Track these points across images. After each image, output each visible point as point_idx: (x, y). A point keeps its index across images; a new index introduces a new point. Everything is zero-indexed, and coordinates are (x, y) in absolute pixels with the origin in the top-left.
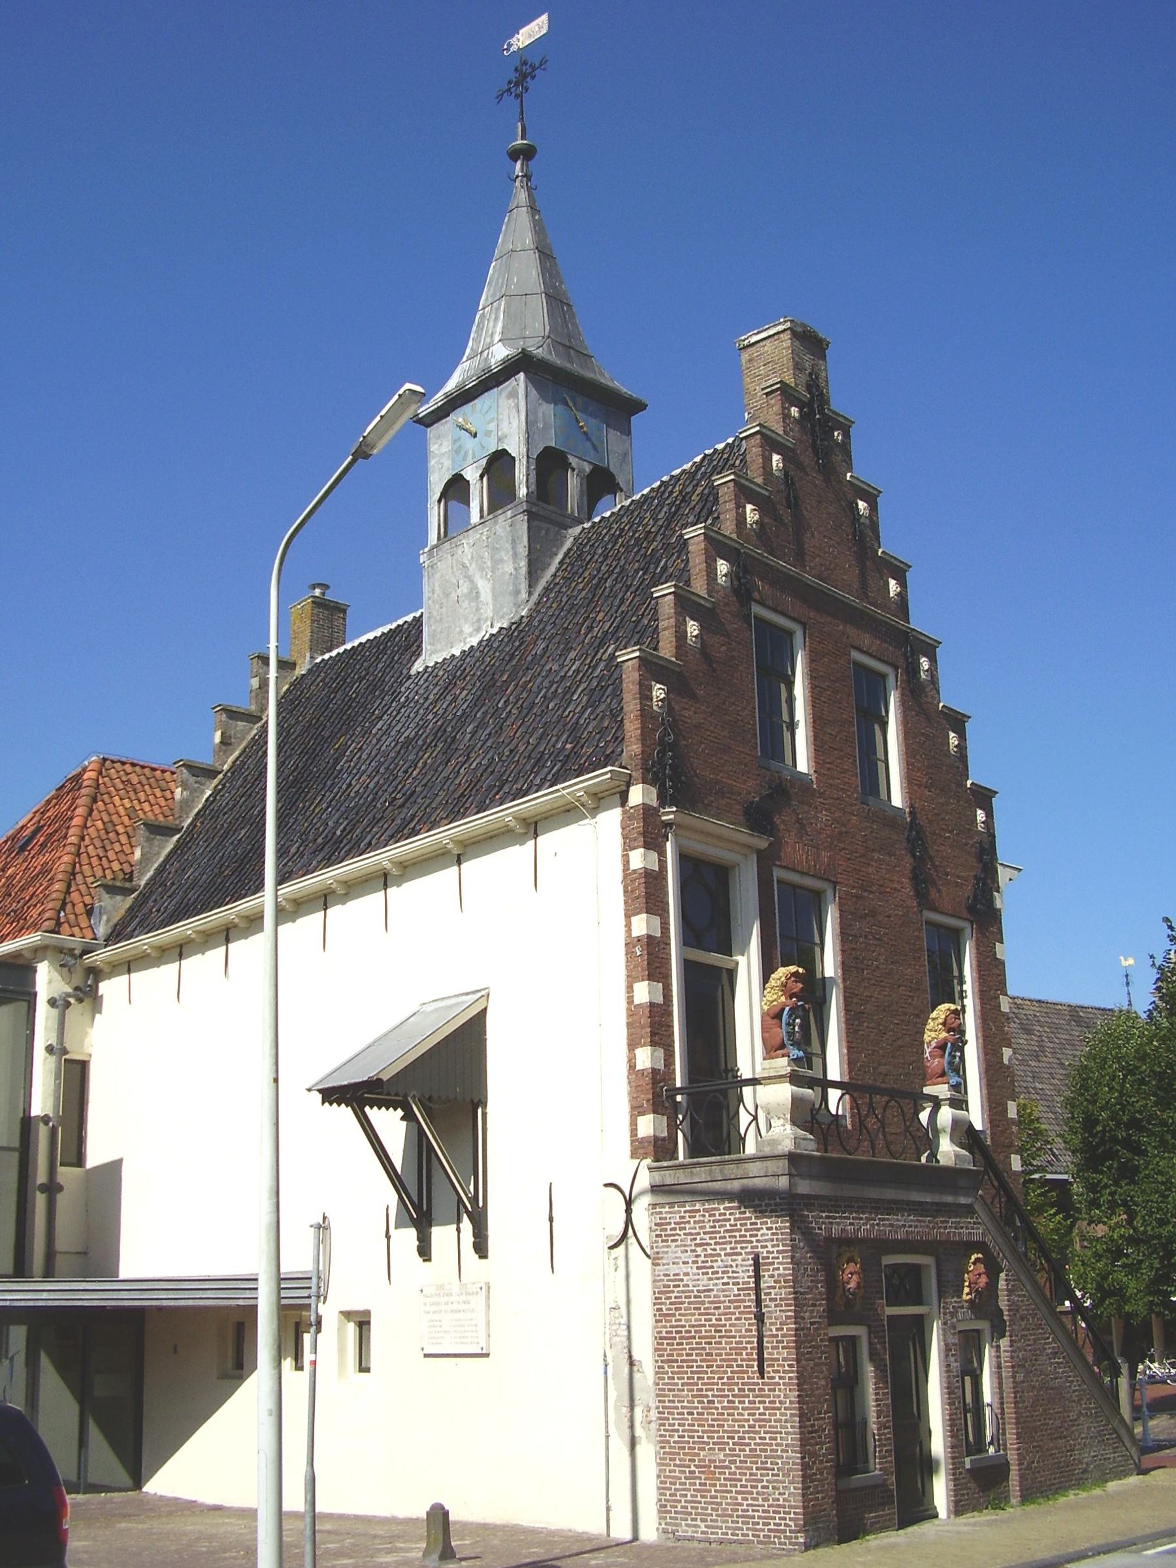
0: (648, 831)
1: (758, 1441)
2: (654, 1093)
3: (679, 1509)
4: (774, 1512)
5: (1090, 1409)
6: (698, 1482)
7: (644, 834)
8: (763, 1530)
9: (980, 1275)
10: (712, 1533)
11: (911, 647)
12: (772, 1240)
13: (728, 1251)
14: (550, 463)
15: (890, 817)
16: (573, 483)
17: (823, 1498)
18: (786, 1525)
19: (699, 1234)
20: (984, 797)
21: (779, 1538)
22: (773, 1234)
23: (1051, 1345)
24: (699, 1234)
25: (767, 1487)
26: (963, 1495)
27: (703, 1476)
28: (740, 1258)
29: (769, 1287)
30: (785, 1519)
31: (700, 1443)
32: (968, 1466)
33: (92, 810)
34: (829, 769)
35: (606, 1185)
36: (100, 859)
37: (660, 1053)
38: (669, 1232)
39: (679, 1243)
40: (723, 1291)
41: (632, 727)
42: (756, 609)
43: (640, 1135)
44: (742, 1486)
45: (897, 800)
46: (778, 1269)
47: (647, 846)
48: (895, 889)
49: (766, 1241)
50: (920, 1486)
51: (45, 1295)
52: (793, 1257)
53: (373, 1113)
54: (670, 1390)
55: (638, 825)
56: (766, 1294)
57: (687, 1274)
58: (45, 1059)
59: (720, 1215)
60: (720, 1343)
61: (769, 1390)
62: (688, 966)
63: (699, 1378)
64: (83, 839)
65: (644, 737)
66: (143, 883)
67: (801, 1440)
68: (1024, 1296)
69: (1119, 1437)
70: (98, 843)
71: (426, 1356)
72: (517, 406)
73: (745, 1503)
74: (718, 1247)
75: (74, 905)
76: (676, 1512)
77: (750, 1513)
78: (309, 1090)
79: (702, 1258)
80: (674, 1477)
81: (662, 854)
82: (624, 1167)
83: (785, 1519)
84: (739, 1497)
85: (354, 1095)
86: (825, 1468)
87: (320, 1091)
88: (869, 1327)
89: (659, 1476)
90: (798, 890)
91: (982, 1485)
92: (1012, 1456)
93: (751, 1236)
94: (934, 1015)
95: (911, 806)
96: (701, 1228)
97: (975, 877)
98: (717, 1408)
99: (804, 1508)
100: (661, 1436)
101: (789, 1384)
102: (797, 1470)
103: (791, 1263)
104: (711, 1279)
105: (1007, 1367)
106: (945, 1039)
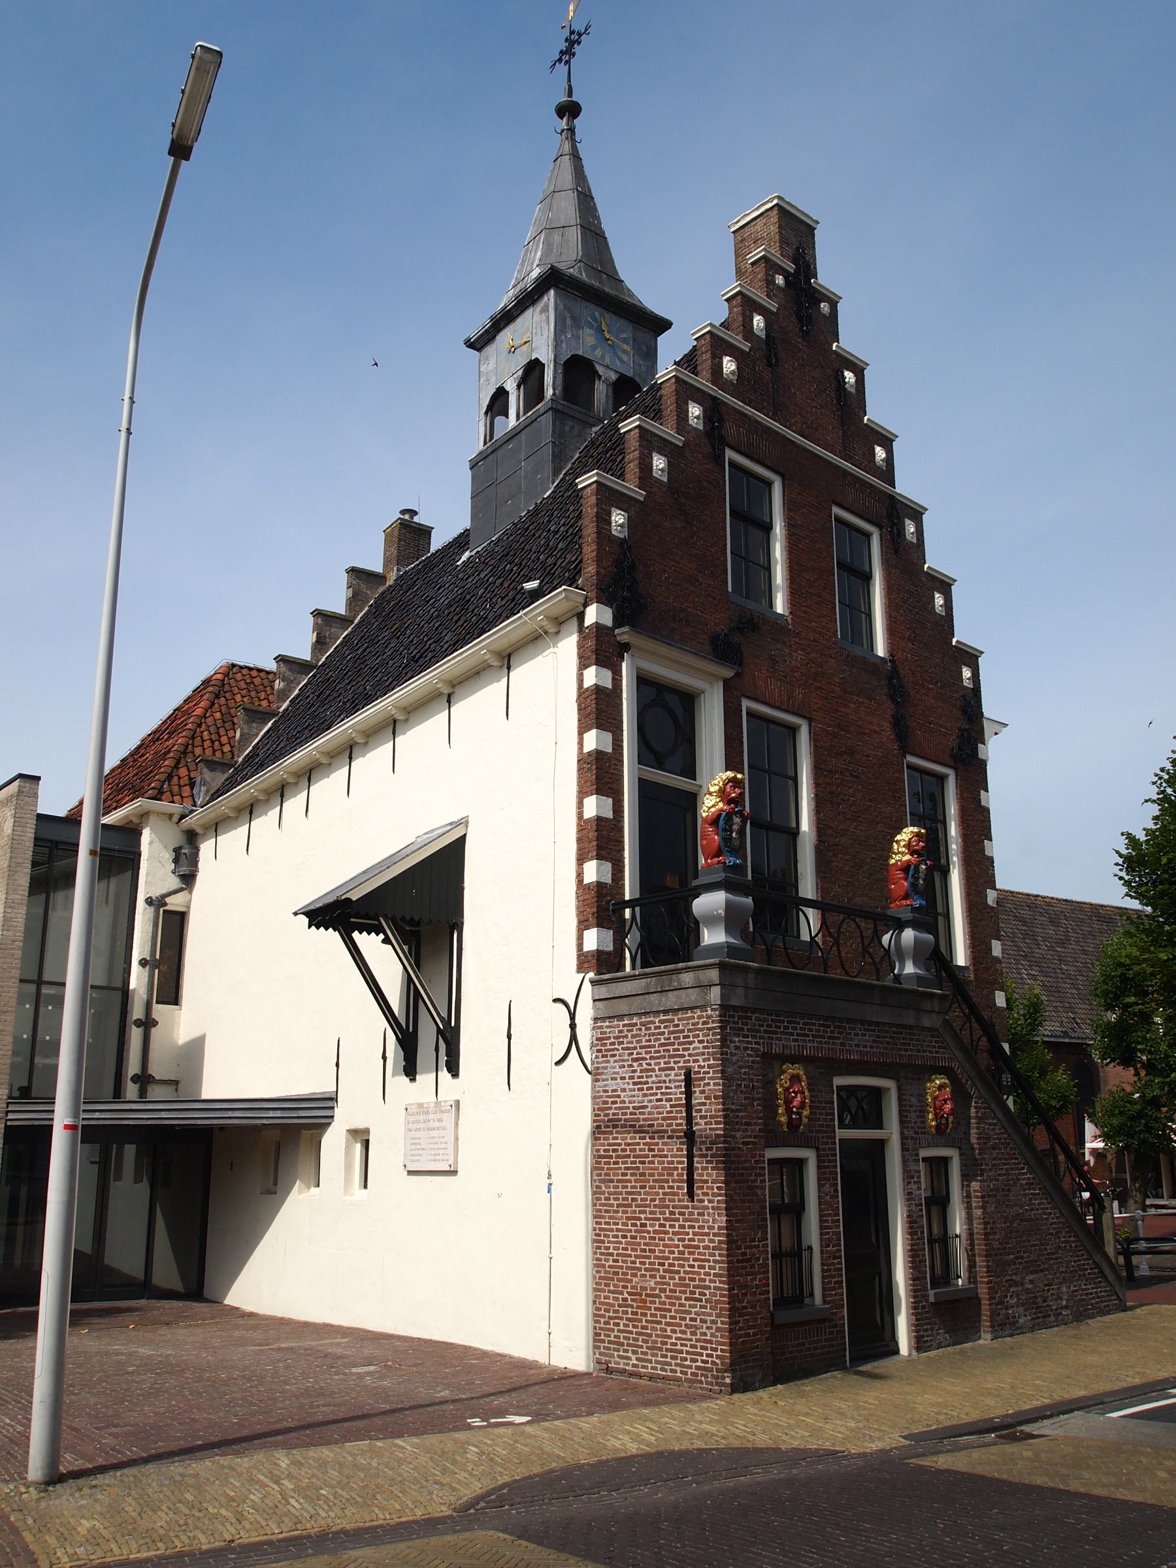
0: (601, 649)
1: (687, 1269)
2: (600, 906)
3: (612, 1338)
4: (702, 1348)
5: (1068, 1242)
6: (630, 1310)
7: (597, 651)
8: (691, 1367)
9: (945, 1100)
10: (643, 1367)
11: (896, 514)
12: (703, 1054)
13: (662, 1065)
14: (577, 371)
15: (872, 665)
16: (601, 391)
17: (755, 1334)
18: (713, 1363)
19: (635, 1048)
20: (971, 657)
21: (706, 1377)
22: (704, 1047)
23: (1026, 1176)
24: (635, 1048)
25: (695, 1320)
26: (926, 1330)
27: (635, 1305)
28: (673, 1073)
29: (700, 1104)
30: (711, 1356)
31: (632, 1268)
32: (932, 1300)
33: (213, 704)
34: (805, 612)
35: (555, 1000)
36: (213, 742)
37: (608, 866)
38: (609, 1047)
39: (617, 1058)
40: (657, 1107)
41: (589, 551)
42: (729, 454)
43: (585, 949)
44: (671, 1317)
45: (881, 650)
46: (708, 1084)
47: (599, 663)
48: (875, 731)
49: (697, 1054)
50: (878, 1319)
51: (97, 1115)
52: (723, 1072)
53: (362, 939)
54: (606, 1211)
55: (591, 643)
56: (697, 1111)
57: (624, 1090)
58: (145, 909)
59: (656, 1028)
60: (653, 1162)
61: (699, 1214)
62: (645, 788)
63: (633, 1200)
64: (200, 725)
65: (599, 560)
66: (241, 759)
67: (729, 1269)
68: (995, 1124)
69: (1102, 1272)
70: (212, 729)
71: (410, 1173)
72: (548, 318)
73: (674, 1336)
74: (653, 1062)
75: (180, 778)
76: (610, 1342)
77: (679, 1347)
78: (296, 914)
79: (638, 1074)
80: (608, 1304)
81: (617, 674)
82: (569, 979)
83: (711, 1356)
84: (669, 1329)
85: (337, 915)
86: (758, 1301)
87: (306, 914)
88: (817, 1149)
89: (594, 1302)
90: (771, 726)
91: (950, 1317)
92: (983, 1291)
93: (684, 1050)
94: (898, 837)
95: (891, 655)
96: (638, 1042)
97: (960, 729)
98: (649, 1232)
99: (731, 1344)
100: (597, 1259)
101: (718, 1208)
102: (723, 1302)
103: (721, 1078)
104: (645, 1095)
105: (977, 1197)
106: (909, 861)
